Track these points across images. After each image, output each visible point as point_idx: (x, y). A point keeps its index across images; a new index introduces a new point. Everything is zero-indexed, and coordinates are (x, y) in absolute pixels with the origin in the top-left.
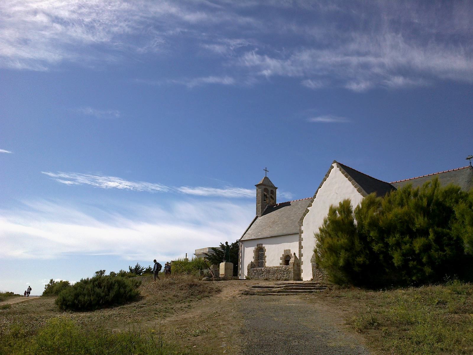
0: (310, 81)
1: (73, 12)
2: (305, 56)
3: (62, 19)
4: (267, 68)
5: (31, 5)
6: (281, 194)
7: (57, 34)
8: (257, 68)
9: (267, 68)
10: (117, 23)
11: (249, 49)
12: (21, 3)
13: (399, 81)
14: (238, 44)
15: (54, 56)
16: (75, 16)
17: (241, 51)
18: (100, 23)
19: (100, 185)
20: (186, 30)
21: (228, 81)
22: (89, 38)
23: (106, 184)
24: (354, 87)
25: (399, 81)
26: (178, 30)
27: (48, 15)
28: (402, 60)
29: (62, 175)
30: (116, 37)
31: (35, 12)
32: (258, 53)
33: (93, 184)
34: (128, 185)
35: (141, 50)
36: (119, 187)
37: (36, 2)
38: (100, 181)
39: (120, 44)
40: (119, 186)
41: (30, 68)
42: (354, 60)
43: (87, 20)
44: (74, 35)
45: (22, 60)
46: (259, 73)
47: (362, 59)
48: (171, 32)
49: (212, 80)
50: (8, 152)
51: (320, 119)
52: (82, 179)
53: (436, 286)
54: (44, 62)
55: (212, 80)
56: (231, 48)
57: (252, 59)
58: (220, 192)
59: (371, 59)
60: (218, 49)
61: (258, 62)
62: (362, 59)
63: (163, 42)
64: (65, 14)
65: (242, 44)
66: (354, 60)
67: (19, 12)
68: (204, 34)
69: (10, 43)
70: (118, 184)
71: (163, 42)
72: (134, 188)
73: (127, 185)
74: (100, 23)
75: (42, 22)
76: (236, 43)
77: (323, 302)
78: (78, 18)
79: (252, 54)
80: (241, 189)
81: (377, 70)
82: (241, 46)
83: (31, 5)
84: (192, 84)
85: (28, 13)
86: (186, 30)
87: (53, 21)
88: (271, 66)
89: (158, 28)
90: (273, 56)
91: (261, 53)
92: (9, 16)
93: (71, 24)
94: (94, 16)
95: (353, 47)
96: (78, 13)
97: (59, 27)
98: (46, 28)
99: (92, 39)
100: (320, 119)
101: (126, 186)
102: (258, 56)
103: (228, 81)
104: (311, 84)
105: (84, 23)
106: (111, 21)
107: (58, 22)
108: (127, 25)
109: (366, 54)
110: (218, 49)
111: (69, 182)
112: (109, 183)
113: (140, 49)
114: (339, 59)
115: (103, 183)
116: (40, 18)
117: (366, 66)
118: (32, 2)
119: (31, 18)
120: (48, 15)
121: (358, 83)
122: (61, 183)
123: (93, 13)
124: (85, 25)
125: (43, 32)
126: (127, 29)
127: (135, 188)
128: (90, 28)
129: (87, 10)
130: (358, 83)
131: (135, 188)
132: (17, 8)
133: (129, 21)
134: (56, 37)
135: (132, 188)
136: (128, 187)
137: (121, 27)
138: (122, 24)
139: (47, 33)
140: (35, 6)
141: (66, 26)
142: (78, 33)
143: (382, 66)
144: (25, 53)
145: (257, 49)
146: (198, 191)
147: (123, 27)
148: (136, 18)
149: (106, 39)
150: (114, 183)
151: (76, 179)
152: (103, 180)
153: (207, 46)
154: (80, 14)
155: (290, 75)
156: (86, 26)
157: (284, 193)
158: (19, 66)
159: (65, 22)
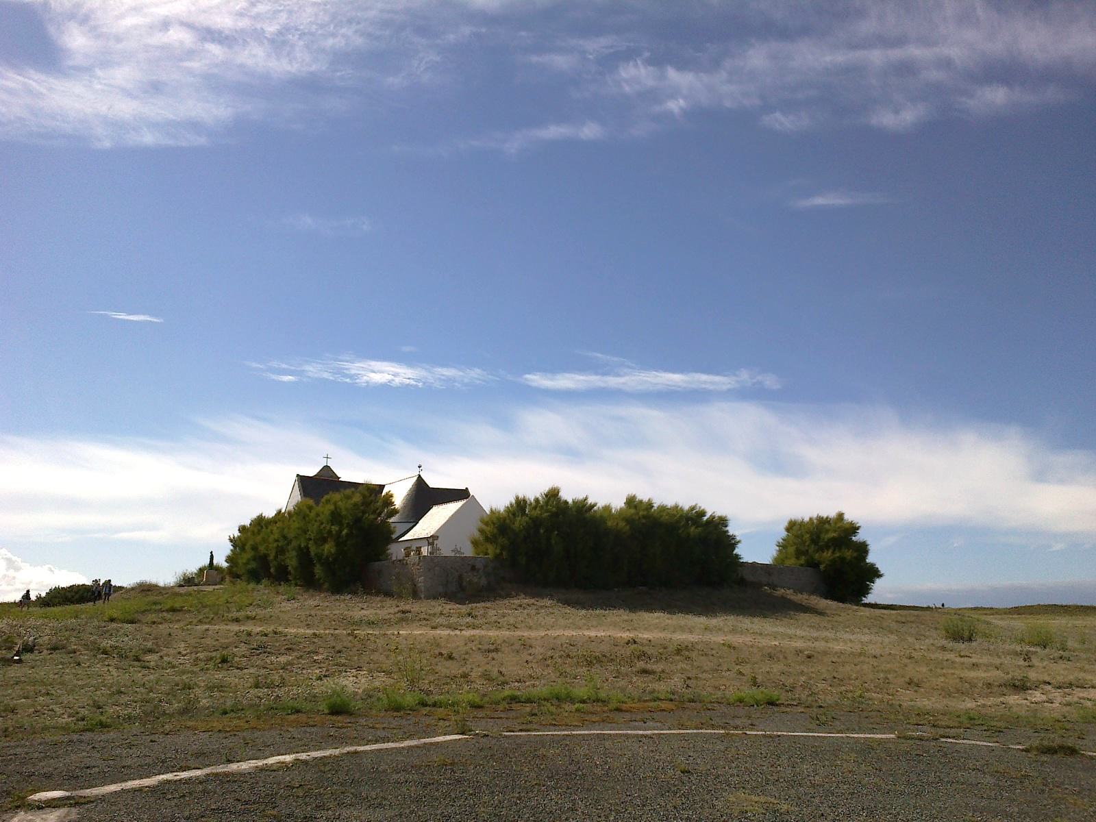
0: (778, 115)
1: (241, 14)
2: (757, 57)
3: (220, 32)
4: (674, 94)
5: (154, 10)
6: (754, 381)
7: (217, 65)
8: (652, 96)
9: (674, 94)
10: (334, 28)
11: (629, 55)
12: (136, 10)
13: (997, 96)
14: (603, 47)
15: (214, 111)
16: (244, 23)
17: (611, 61)
18: (299, 33)
19: (354, 381)
20: (484, 30)
21: (590, 131)
22: (282, 67)
23: (365, 378)
24: (886, 119)
25: (997, 96)
26: (466, 30)
27: (188, 25)
28: (996, 47)
29: (275, 364)
30: (340, 58)
31: (165, 25)
32: (649, 62)
33: (340, 379)
34: (413, 379)
35: (394, 81)
36: (394, 383)
37: (165, 3)
38: (353, 372)
39: (349, 74)
40: (393, 380)
41: (171, 142)
42: (876, 57)
43: (271, 29)
44: (250, 62)
45: (154, 126)
46: (657, 109)
47: (896, 54)
48: (451, 37)
49: (554, 132)
50: (155, 320)
51: (819, 201)
52: (313, 370)
53: (776, 591)
54: (195, 126)
55: (554, 132)
56: (591, 57)
57: (636, 75)
58: (613, 381)
59: (915, 52)
60: (561, 62)
61: (650, 83)
62: (896, 54)
63: (438, 59)
64: (224, 22)
65: (611, 47)
66: (876, 57)
67: (136, 27)
68: (523, 34)
69: (128, 93)
70: (390, 377)
71: (438, 59)
72: (424, 383)
73: (409, 379)
74: (299, 33)
75: (181, 42)
76: (595, 46)
77: (555, 644)
78: (253, 28)
79: (636, 66)
80: (659, 374)
81: (935, 75)
82: (612, 51)
83: (154, 10)
84: (514, 144)
85: (151, 28)
86: (484, 30)
87: (204, 39)
88: (683, 88)
89: (422, 31)
90: (682, 66)
91: (658, 61)
92: (118, 39)
93: (241, 41)
94: (283, 18)
95: (867, 27)
96: (250, 17)
97: (215, 50)
98: (190, 54)
99: (289, 68)
100: (819, 201)
101: (408, 380)
102: (651, 68)
103: (590, 131)
104: (781, 121)
105: (266, 35)
106: (322, 26)
107: (213, 41)
108: (356, 32)
109: (900, 41)
110: (561, 62)
111: (290, 377)
112: (372, 375)
113: (390, 80)
114: (841, 57)
115: (359, 376)
116: (177, 36)
117: (906, 69)
118: (156, 5)
119: (159, 39)
120: (188, 25)
121: (896, 112)
122: (273, 380)
123: (280, 11)
124: (268, 39)
125: (188, 64)
126: (359, 41)
127: (427, 384)
128: (279, 43)
129: (268, 7)
130: (896, 112)
131: (427, 384)
132: (130, 21)
133: (359, 23)
134: (216, 71)
135: (420, 385)
136: (413, 382)
137: (343, 36)
138: (344, 30)
139: (195, 65)
140: (163, 11)
141: (230, 47)
142: (255, 57)
143: (946, 64)
144: (159, 109)
145: (647, 54)
146: (566, 381)
147: (348, 38)
148: (372, 14)
149: (319, 66)
150: (381, 373)
151: (303, 371)
152: (357, 370)
153: (535, 59)
154: (257, 17)
155: (728, 104)
156: (272, 41)
157: (760, 378)
158: (148, 139)
159: (227, 38)
